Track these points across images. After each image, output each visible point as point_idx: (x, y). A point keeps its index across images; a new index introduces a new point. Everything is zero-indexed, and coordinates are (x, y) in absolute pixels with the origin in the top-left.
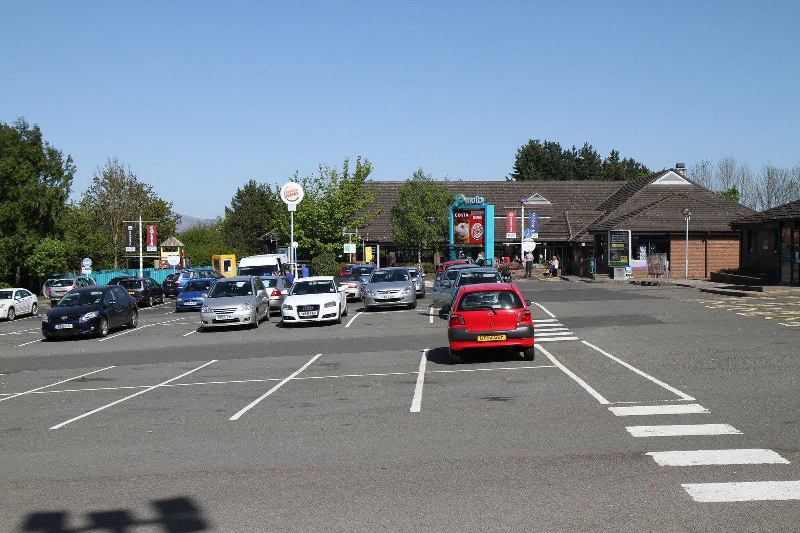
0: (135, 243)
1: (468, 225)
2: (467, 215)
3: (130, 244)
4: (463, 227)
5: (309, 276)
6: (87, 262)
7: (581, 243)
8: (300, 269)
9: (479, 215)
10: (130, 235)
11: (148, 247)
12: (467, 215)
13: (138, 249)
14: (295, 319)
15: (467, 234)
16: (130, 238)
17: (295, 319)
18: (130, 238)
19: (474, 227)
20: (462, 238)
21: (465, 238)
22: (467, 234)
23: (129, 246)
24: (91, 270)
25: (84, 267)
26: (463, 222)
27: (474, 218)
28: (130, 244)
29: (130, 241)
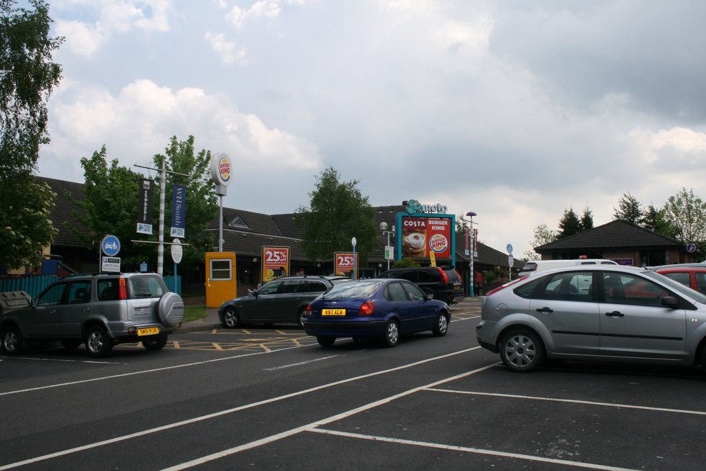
0: (153, 218)
1: (424, 236)
2: (423, 224)
3: (145, 219)
4: (416, 238)
5: (205, 295)
6: (111, 245)
7: (378, 264)
8: (363, 273)
9: (441, 225)
10: (146, 200)
11: (172, 228)
12: (423, 224)
13: (156, 228)
14: (516, 291)
15: (423, 246)
16: (146, 204)
17: (516, 291)
18: (146, 204)
19: (433, 238)
20: (417, 251)
21: (419, 251)
22: (423, 246)
23: (142, 222)
24: (119, 265)
25: (104, 255)
26: (416, 232)
27: (433, 228)
28: (145, 219)
29: (145, 212)
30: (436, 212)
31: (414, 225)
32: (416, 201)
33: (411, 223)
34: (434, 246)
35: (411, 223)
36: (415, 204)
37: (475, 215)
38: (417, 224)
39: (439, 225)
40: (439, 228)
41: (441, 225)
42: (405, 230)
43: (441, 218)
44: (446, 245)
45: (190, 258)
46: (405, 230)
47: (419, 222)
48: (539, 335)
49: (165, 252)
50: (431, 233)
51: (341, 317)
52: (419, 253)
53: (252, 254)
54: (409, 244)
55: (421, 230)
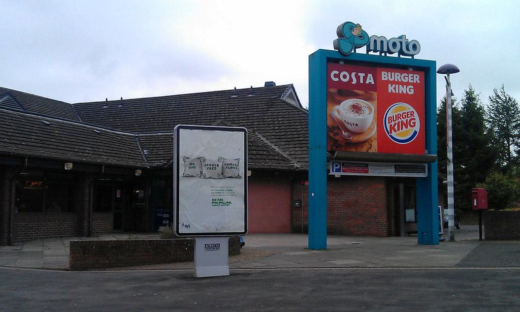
1: (373, 106)
2: (370, 79)
4: (356, 109)
9: (408, 84)
12: (370, 79)
15: (370, 129)
19: (392, 112)
20: (355, 139)
21: (362, 138)
22: (370, 129)
26: (357, 96)
27: (391, 88)
30: (396, 55)
31: (351, 79)
32: (359, 26)
33: (345, 77)
34: (392, 128)
35: (345, 77)
36: (356, 32)
37: (456, 70)
38: (358, 78)
39: (402, 84)
40: (403, 90)
41: (408, 84)
42: (332, 90)
43: (402, 67)
44: (417, 128)
45: (370, 151)
46: (332, 90)
47: (362, 75)
48: (333, 235)
49: (446, 165)
50: (386, 101)
51: (33, 182)
52: (361, 143)
53: (131, 163)
54: (341, 123)
55: (366, 91)
